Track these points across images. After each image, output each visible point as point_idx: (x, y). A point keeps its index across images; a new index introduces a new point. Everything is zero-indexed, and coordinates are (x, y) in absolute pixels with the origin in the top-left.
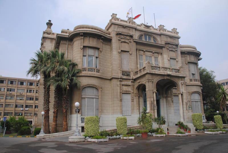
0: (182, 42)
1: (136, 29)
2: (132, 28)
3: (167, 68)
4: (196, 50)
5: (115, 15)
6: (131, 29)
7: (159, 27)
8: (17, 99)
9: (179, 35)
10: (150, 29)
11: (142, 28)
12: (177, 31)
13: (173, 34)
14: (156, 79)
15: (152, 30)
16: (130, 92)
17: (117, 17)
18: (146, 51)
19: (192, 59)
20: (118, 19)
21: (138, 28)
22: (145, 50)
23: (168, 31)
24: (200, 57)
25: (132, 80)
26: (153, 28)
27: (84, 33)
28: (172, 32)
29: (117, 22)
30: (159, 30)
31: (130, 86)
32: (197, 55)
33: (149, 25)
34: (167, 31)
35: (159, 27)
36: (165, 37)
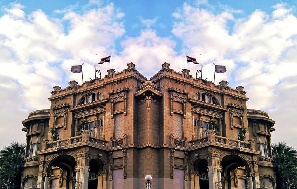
0: (250, 106)
1: (192, 86)
2: (188, 84)
3: (234, 141)
4: (268, 117)
5: (241, 88)
6: (186, 85)
7: (220, 83)
8: (152, 171)
9: (247, 95)
10: (209, 86)
11: (200, 84)
12: (244, 90)
13: (183, 78)
14: (225, 154)
15: (212, 88)
16: (121, 167)
17: (171, 67)
18: (204, 115)
19: (262, 129)
20: (171, 71)
21: (195, 83)
22: (201, 114)
23: (176, 73)
24: (272, 127)
25: (186, 151)
26: (36, 27)
27: (257, 120)
28: (182, 75)
29: (169, 74)
30: (221, 88)
31: (122, 157)
32: (269, 124)
33: (208, 80)
34: (232, 90)
35: (220, 83)
36: (228, 97)
